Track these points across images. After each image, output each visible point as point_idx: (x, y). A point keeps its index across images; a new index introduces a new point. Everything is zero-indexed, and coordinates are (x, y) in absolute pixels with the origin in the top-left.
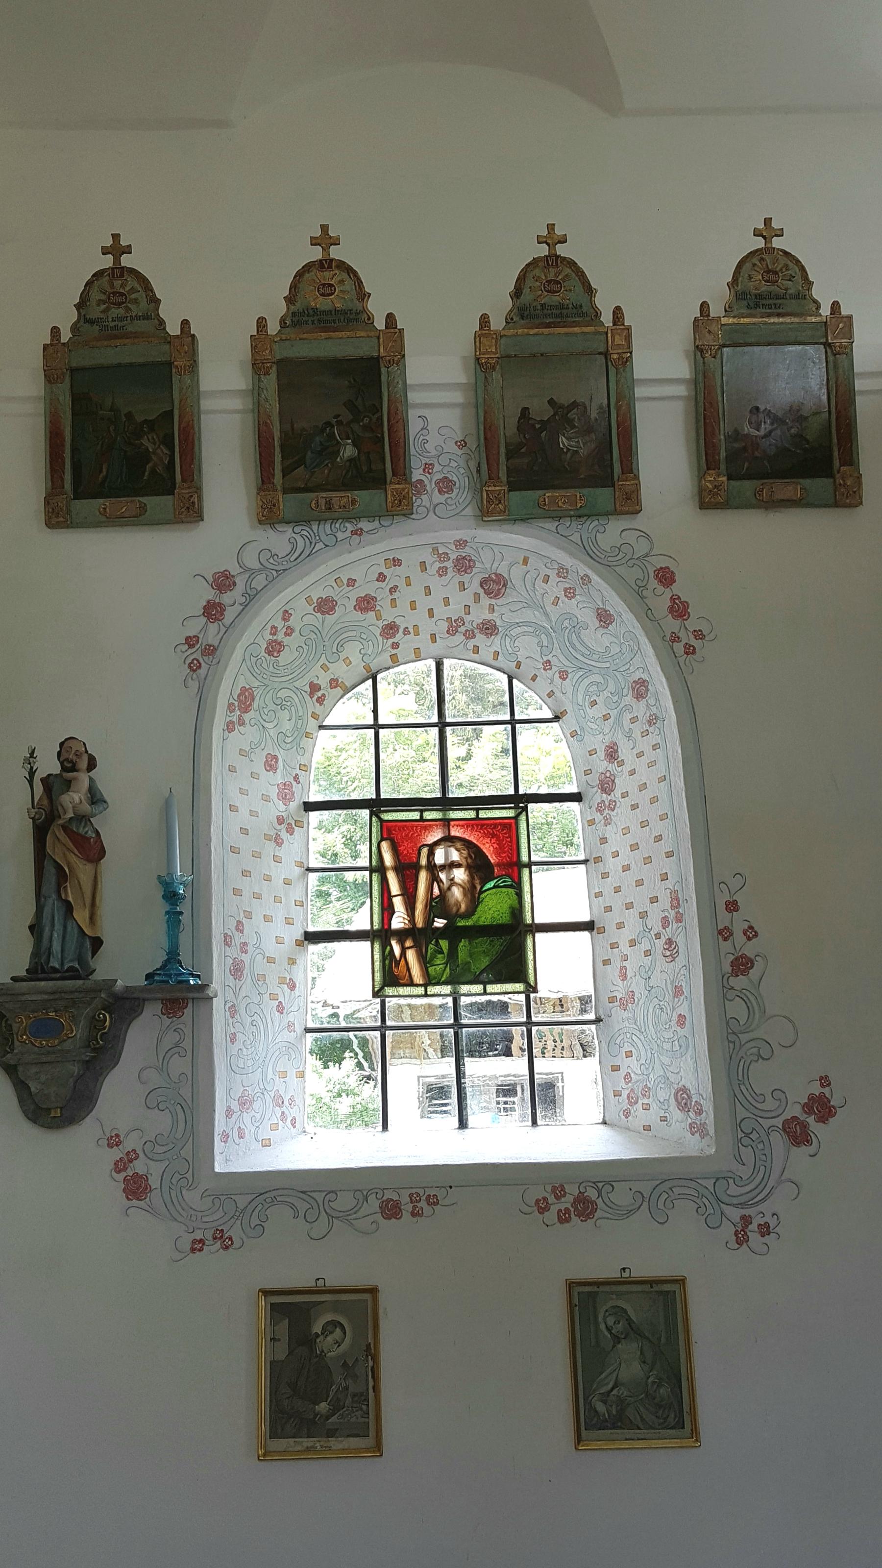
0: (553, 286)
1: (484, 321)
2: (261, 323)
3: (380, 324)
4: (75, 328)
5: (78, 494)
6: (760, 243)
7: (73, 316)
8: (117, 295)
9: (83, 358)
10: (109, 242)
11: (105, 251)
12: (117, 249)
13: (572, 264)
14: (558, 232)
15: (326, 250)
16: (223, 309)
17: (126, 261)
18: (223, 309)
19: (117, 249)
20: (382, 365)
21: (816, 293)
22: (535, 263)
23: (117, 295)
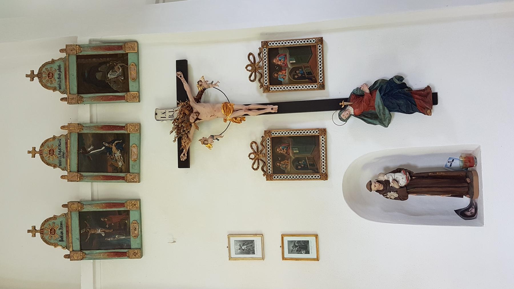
0: (53, 231)
1: (66, 256)
2: (63, 177)
3: (64, 55)
4: (62, 93)
5: (127, 90)
6: (36, 79)
7: (57, 92)
8: (50, 232)
9: (77, 245)
10: (31, 234)
11: (34, 236)
12: (33, 231)
13: (43, 224)
14: (31, 150)
15: (36, 231)
16: (57, 191)
17: (38, 228)
18: (57, 191)
19: (33, 231)
20: (80, 54)
21: (58, 135)
22: (41, 82)
23: (50, 232)
